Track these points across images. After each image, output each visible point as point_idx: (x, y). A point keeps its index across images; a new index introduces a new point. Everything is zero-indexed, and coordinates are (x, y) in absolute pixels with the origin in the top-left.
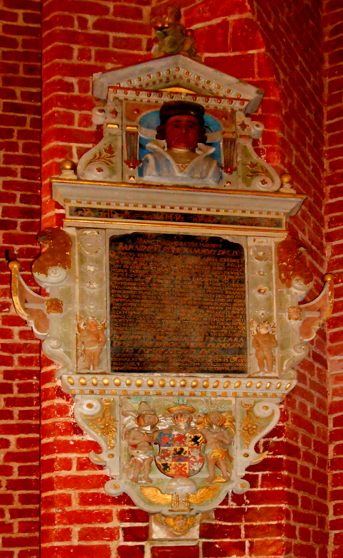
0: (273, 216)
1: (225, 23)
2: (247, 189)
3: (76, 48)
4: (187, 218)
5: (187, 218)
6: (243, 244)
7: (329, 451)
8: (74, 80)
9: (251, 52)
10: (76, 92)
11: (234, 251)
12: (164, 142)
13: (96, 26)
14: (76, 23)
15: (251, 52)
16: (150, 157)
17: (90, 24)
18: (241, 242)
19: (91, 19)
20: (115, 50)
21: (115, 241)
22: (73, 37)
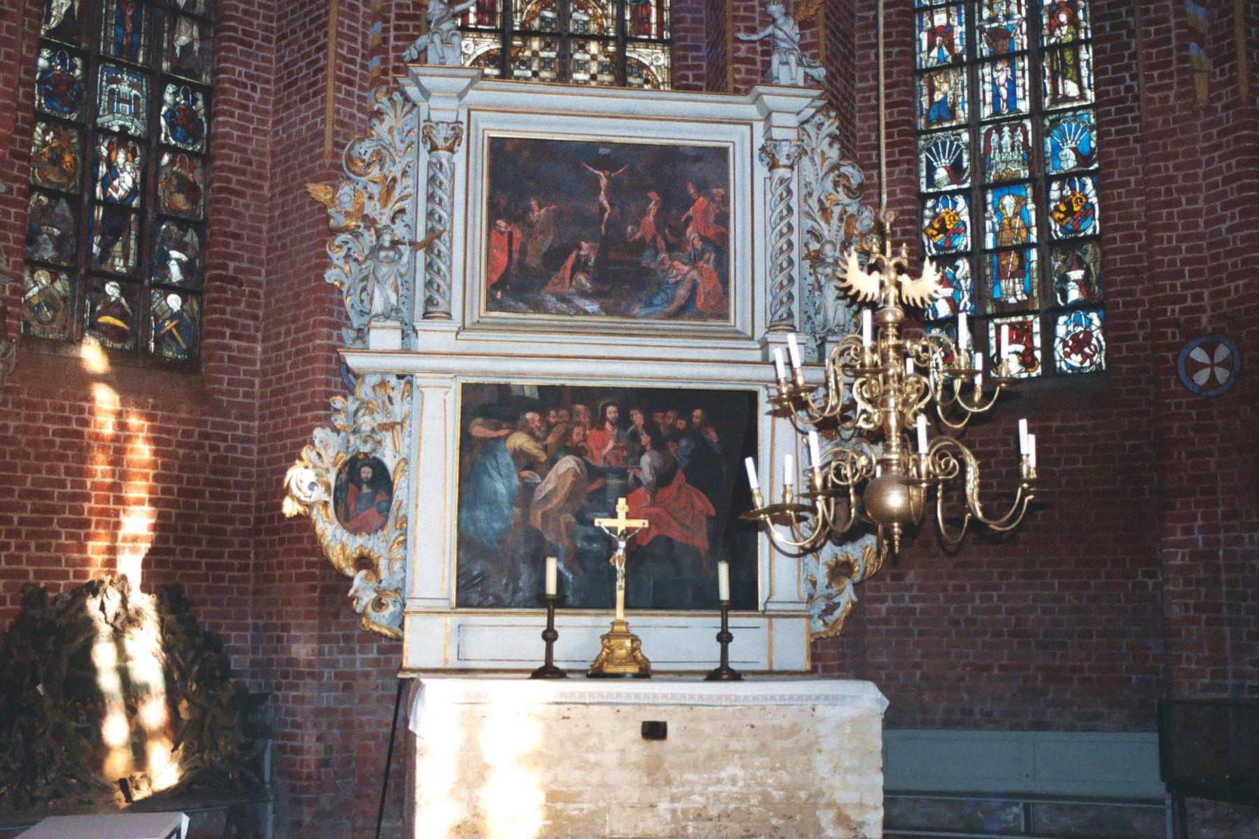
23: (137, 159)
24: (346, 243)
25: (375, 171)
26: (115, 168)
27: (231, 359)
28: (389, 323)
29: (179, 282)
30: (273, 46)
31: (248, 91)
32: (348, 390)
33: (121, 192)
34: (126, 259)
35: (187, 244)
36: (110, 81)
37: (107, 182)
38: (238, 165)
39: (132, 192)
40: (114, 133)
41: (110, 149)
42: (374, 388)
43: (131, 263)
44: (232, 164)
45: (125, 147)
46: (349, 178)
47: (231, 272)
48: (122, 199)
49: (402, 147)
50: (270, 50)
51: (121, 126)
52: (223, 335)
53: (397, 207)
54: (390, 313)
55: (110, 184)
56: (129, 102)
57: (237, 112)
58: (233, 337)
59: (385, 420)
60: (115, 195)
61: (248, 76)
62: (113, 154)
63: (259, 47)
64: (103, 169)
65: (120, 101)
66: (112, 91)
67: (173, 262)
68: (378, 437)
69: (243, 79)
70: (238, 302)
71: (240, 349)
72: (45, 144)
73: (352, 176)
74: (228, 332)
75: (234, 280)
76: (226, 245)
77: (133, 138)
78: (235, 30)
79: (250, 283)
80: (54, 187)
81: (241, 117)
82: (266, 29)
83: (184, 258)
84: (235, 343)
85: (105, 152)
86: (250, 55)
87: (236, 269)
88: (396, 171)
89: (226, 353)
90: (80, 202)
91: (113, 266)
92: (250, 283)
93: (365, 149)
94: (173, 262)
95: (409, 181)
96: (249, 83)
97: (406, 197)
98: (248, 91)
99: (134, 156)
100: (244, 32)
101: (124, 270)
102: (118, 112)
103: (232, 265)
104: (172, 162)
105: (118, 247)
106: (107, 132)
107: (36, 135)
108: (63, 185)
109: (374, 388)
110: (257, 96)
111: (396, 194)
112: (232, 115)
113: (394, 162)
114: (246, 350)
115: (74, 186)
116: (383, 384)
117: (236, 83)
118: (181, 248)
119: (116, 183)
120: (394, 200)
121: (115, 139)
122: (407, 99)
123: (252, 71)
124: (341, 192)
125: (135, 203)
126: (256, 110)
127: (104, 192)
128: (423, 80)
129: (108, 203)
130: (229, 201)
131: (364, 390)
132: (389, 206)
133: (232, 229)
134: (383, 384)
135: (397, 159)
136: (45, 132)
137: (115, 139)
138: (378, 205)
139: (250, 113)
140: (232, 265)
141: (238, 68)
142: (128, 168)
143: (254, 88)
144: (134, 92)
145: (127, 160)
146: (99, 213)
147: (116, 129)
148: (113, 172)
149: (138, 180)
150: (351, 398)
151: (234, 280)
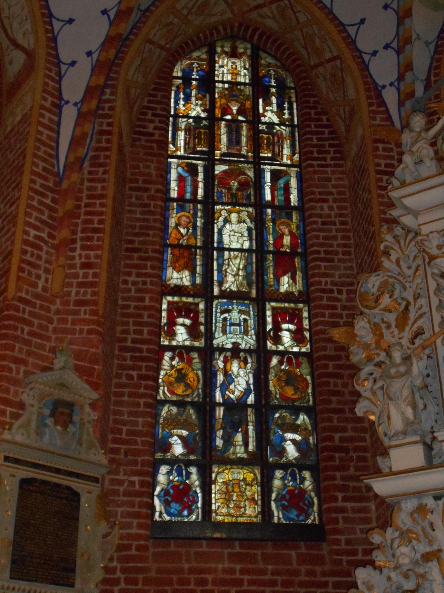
0: (95, 475)
1: (87, 352)
2: (95, 132)
3: (18, 345)
4: (58, 471)
5: (58, 471)
6: (81, 493)
7: (69, 399)
8: (13, 366)
9: (96, 367)
10: (14, 374)
11: (74, 497)
12: (53, 419)
13: (29, 333)
14: (20, 330)
15: (96, 367)
16: (47, 430)
17: (25, 332)
18: (79, 491)
19: (27, 329)
20: (35, 350)
21: (23, 482)
22: (16, 338)
23: (249, 365)
24: (371, 374)
25: (386, 300)
26: (230, 375)
27: (346, 520)
28: (408, 439)
29: (296, 459)
30: (353, 256)
31: (336, 294)
32: (385, 523)
33: (237, 393)
34: (246, 444)
35: (299, 426)
36: (222, 312)
37: (225, 387)
38: (333, 353)
39: (247, 392)
40: (227, 350)
41: (225, 361)
42: (411, 514)
43: (251, 448)
44: (327, 353)
45: (238, 357)
46: (362, 313)
47: (337, 442)
48: (239, 399)
49: (410, 272)
50: (350, 261)
51: (233, 344)
52: (335, 499)
53: (415, 328)
54: (409, 427)
55: (227, 388)
56: (239, 325)
57: (327, 312)
58: (345, 499)
59: (428, 549)
60: (232, 396)
61: (334, 284)
62: (228, 365)
63: (340, 261)
64: (220, 378)
65: (232, 324)
66: (225, 319)
67: (289, 442)
68: (421, 571)
69: (329, 287)
70: (347, 468)
71: (354, 510)
72: (172, 367)
73: (366, 311)
74: (340, 495)
75: (340, 449)
76: (330, 419)
77: (244, 351)
78: (318, 252)
79: (357, 449)
80: (180, 399)
81: (332, 316)
82: (345, 246)
83: (298, 438)
84: (348, 505)
85: (221, 365)
86: (333, 268)
87: (342, 439)
88: (409, 295)
89: (340, 516)
90: (205, 407)
91: (235, 453)
92: (357, 449)
93: (372, 283)
94: (289, 442)
95: (422, 301)
96: (335, 288)
97: (421, 316)
98: (336, 294)
99: (246, 362)
100: (326, 252)
101: (245, 456)
102: (230, 333)
103: (337, 436)
104: (281, 362)
105: (239, 437)
106: (222, 350)
107: (164, 362)
108: (188, 396)
109: (411, 514)
110: (344, 296)
111: (412, 315)
112: (323, 315)
113: (405, 288)
114: (359, 510)
115: (198, 395)
116: (421, 510)
117: (323, 291)
118: (295, 429)
119: (232, 387)
120: (410, 322)
121: (229, 354)
122: (408, 231)
123: (337, 279)
124: (357, 327)
125: (251, 399)
126: (344, 308)
127: (223, 395)
128: (407, 202)
129: (228, 404)
130: (328, 384)
131: (403, 519)
132: (407, 329)
133: (333, 406)
134: (421, 510)
135: (407, 285)
136: (172, 359)
137: (229, 354)
138: (396, 331)
139: (339, 311)
140: (337, 436)
141: (324, 280)
142: (242, 373)
143: (340, 292)
144: (243, 316)
145: (240, 367)
146: (220, 412)
147: (229, 346)
148: (229, 378)
149: (251, 381)
150: (389, 530)
151: (340, 449)
